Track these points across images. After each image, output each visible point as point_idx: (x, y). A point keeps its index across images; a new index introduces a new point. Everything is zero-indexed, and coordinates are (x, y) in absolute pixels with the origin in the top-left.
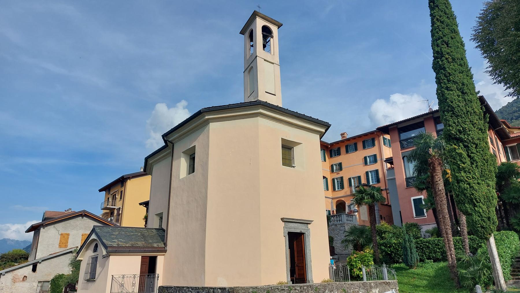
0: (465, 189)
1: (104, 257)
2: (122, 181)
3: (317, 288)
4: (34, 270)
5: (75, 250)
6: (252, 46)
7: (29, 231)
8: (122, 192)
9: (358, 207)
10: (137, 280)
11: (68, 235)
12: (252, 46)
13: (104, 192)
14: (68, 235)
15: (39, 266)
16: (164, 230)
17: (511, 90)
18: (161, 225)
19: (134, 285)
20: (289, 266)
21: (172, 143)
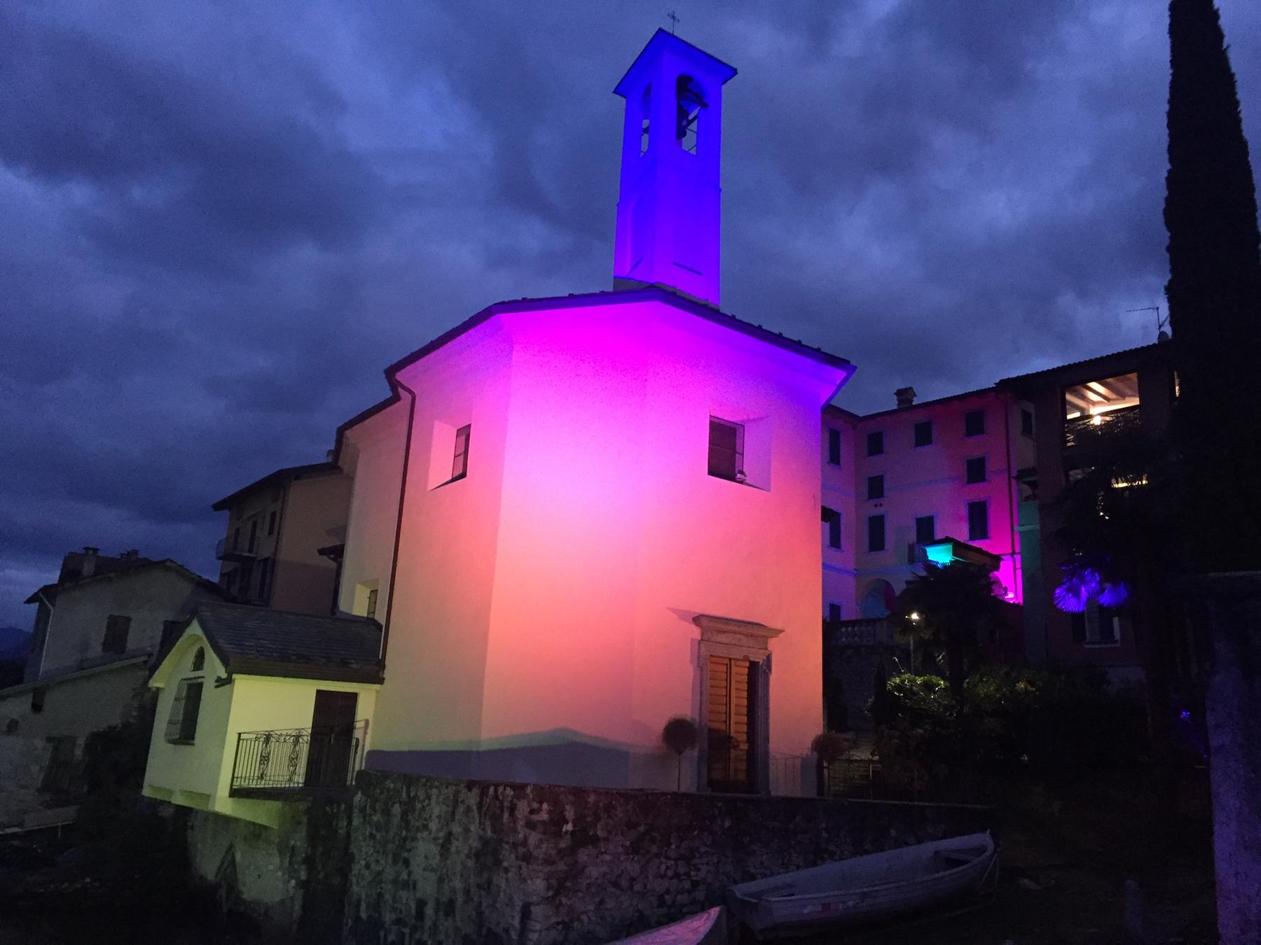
0: (567, 926)
1: (221, 683)
2: (278, 483)
3: (711, 783)
4: (37, 708)
5: (145, 662)
6: (646, 131)
7: (30, 601)
8: (274, 514)
9: (1101, 607)
10: (304, 749)
11: (129, 619)
12: (646, 131)
13: (226, 513)
14: (129, 619)
15: (51, 699)
16: (379, 626)
17: (1168, 329)
18: (372, 611)
19: (293, 760)
20: (496, 746)
21: (410, 392)
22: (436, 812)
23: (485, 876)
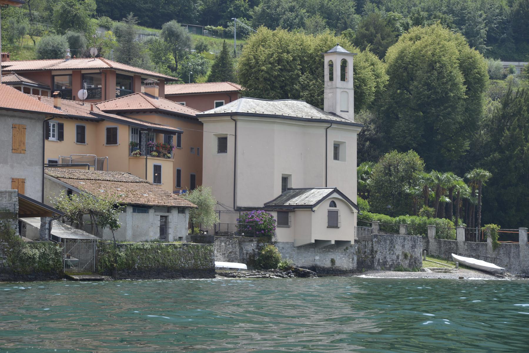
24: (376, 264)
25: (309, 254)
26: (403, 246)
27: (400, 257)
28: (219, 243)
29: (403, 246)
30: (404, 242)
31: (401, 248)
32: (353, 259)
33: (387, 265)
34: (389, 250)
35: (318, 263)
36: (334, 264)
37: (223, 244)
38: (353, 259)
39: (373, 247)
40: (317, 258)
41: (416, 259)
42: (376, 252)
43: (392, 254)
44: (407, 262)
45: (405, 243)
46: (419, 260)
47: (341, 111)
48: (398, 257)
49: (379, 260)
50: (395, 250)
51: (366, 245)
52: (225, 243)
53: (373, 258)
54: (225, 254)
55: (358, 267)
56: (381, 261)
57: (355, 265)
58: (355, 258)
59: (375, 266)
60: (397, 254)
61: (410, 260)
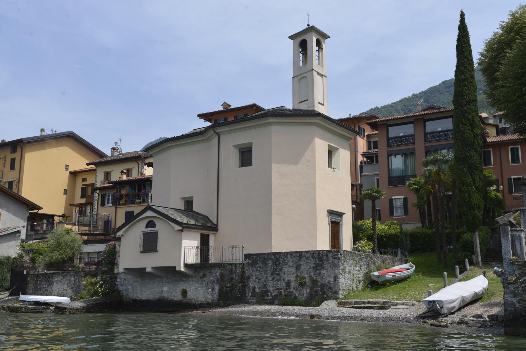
22: (291, 260)
23: (318, 271)
24: (249, 294)
25: (155, 284)
26: (298, 268)
27: (293, 285)
28: (69, 278)
29: (298, 268)
30: (300, 260)
31: (294, 270)
32: (213, 289)
33: (268, 296)
34: (272, 274)
35: (166, 295)
36: (186, 297)
37: (72, 279)
38: (213, 289)
39: (244, 272)
40: (165, 289)
41: (323, 286)
42: (249, 278)
43: (278, 280)
44: (306, 291)
45: (302, 262)
46: (331, 288)
47: (300, 103)
48: (288, 284)
49: (254, 289)
50: (282, 274)
51: (232, 269)
52: (74, 278)
53: (244, 286)
54: (73, 288)
55: (219, 300)
56: (257, 290)
57: (216, 297)
58: (217, 288)
59: (248, 298)
60: (286, 279)
61: (312, 288)
